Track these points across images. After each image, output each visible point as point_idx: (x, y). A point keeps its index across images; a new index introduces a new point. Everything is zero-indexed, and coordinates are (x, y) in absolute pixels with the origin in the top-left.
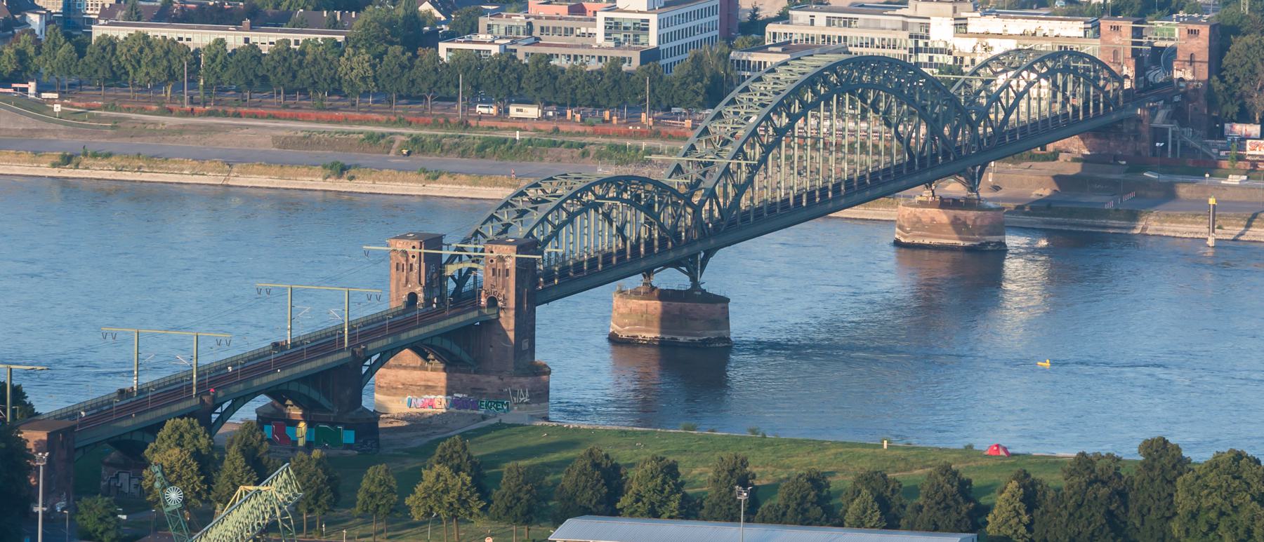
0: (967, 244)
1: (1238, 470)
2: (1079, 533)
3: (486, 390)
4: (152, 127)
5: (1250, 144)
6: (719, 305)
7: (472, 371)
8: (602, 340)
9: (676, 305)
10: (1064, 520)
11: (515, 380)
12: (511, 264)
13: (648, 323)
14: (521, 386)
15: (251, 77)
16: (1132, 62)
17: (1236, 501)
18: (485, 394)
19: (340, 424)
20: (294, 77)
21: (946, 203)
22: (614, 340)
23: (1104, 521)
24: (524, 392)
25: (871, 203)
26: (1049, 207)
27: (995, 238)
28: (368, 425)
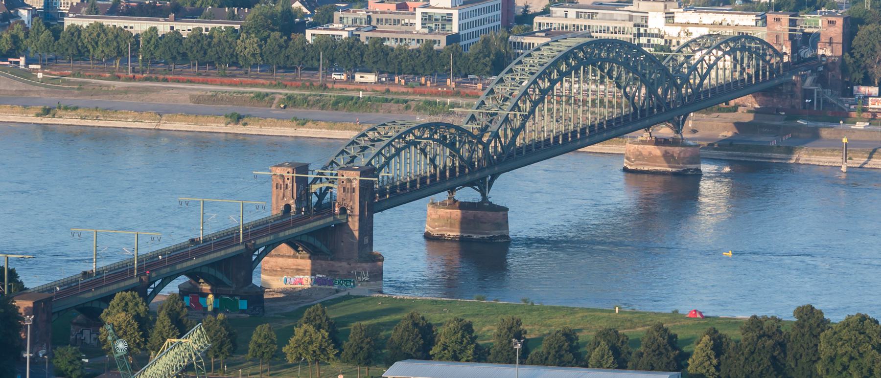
0: (674, 170)
2: (752, 372)
3: (338, 272)
4: (106, 88)
5: (872, 100)
6: (501, 213)
7: (329, 259)
8: (420, 237)
9: (471, 212)
11: (359, 265)
12: (356, 184)
13: (452, 225)
14: (363, 269)
15: (175, 54)
16: (789, 43)
17: (861, 349)
18: (338, 275)
19: (237, 296)
20: (205, 53)
21: (659, 142)
22: (428, 237)
23: (770, 364)
24: (366, 273)
25: (607, 142)
26: (731, 144)
27: (694, 166)
28: (257, 296)
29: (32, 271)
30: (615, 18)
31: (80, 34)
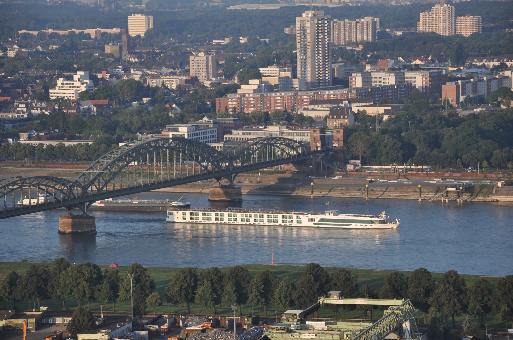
0: (229, 199)
1: (81, 270)
2: (25, 295)
4: (13, 171)
6: (91, 220)
8: (56, 233)
9: (77, 220)
10: (20, 290)
13: (69, 226)
15: (50, 155)
16: (320, 142)
20: (63, 154)
21: (222, 187)
22: (60, 233)
23: (35, 290)
25: (182, 185)
26: (269, 188)
27: (238, 197)
29: (279, 262)
30: (258, 134)
31: (8, 147)
